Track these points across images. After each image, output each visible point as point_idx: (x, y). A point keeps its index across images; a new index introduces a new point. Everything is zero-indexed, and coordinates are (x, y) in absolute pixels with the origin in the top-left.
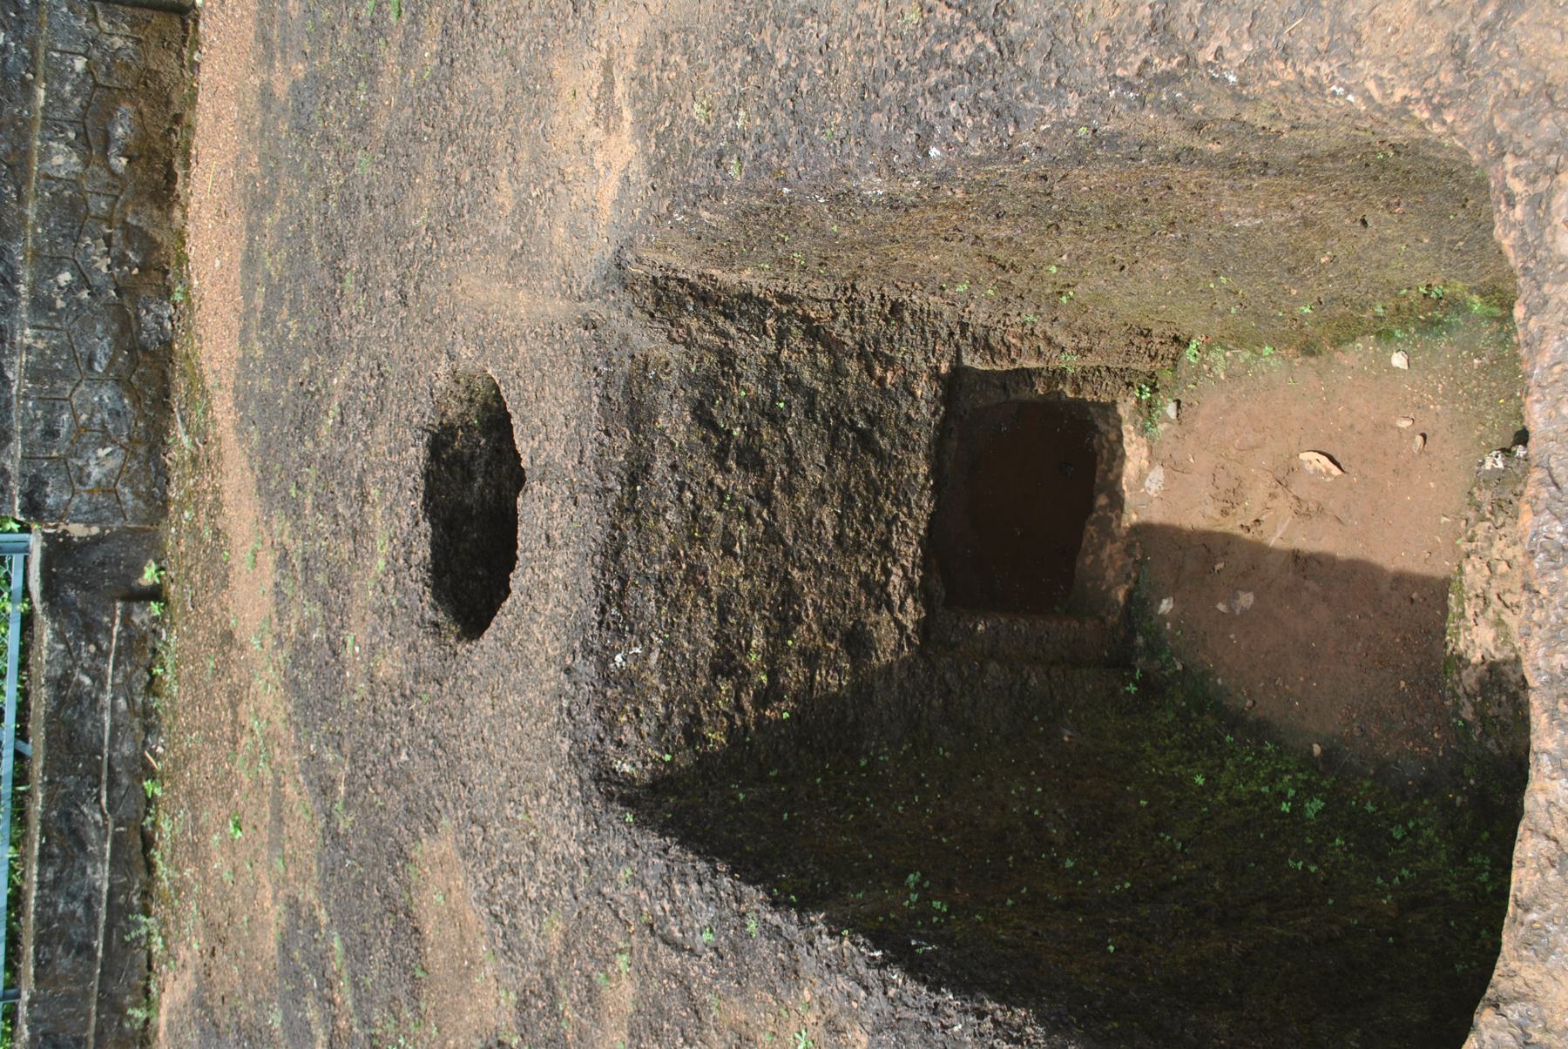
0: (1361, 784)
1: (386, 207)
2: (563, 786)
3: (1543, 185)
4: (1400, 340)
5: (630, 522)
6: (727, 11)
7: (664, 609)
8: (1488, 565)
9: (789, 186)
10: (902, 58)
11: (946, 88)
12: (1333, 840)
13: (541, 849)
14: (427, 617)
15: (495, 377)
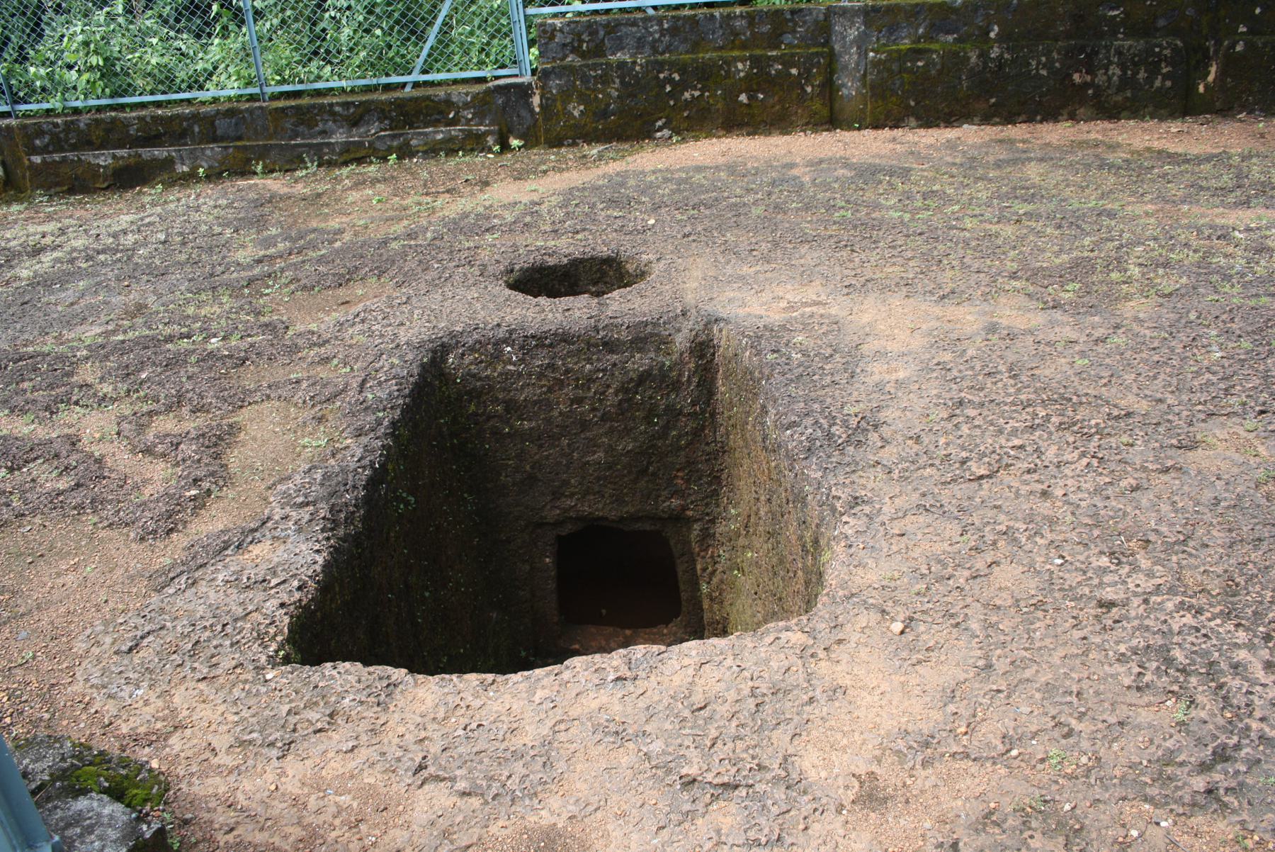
2: (436, 331)
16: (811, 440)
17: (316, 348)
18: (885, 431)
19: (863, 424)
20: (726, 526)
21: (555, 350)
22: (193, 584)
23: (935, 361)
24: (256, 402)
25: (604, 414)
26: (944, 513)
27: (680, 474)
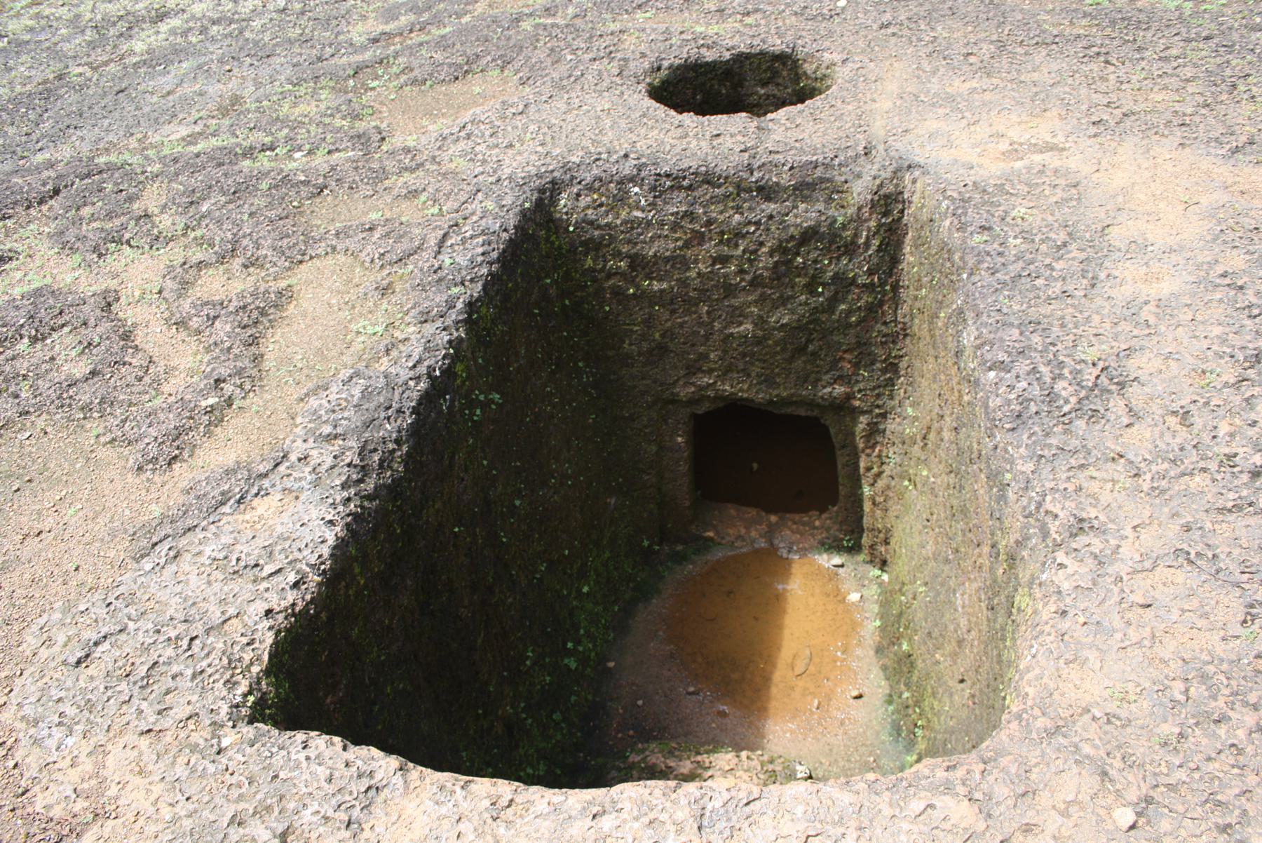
1: (950, 8)
2: (548, 160)
3: (961, 790)
4: (887, 710)
5: (731, 189)
6: (1093, 226)
7: (672, 218)
8: (732, 769)
9: (968, 278)
10: (1059, 347)
12: (549, 675)
13: (507, 150)
14: (664, 62)
15: (831, 91)
16: (1024, 400)
17: (406, 174)
18: (1133, 391)
19: (1104, 380)
20: (899, 424)
21: (695, 193)
22: (175, 557)
23: (1220, 269)
24: (318, 256)
25: (755, 278)
26: (1218, 572)
27: (847, 356)
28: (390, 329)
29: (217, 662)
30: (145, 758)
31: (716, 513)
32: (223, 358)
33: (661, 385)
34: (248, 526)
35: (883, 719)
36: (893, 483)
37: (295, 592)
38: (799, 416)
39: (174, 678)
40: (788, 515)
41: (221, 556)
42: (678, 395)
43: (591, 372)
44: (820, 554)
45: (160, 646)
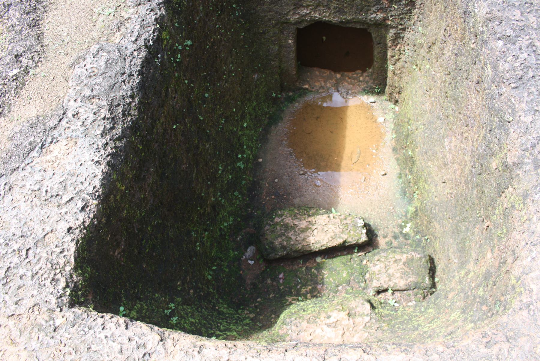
0: (251, 177)
4: (398, 182)
8: (326, 224)
11: (534, 51)
12: (231, 174)
22: (10, 189)
28: (119, 10)
29: (44, 266)
30: (13, 333)
31: (309, 74)
32: (17, 39)
33: (280, 15)
34: (50, 164)
35: (397, 186)
36: (406, 65)
37: (83, 213)
38: (356, 29)
39: (21, 278)
40: (346, 73)
41: (36, 188)
42: (289, 19)
43: (240, 9)
44: (363, 95)
45: (10, 256)
